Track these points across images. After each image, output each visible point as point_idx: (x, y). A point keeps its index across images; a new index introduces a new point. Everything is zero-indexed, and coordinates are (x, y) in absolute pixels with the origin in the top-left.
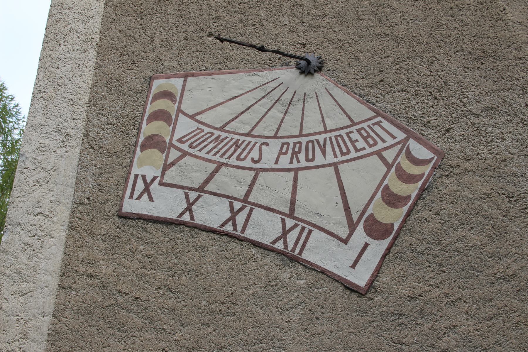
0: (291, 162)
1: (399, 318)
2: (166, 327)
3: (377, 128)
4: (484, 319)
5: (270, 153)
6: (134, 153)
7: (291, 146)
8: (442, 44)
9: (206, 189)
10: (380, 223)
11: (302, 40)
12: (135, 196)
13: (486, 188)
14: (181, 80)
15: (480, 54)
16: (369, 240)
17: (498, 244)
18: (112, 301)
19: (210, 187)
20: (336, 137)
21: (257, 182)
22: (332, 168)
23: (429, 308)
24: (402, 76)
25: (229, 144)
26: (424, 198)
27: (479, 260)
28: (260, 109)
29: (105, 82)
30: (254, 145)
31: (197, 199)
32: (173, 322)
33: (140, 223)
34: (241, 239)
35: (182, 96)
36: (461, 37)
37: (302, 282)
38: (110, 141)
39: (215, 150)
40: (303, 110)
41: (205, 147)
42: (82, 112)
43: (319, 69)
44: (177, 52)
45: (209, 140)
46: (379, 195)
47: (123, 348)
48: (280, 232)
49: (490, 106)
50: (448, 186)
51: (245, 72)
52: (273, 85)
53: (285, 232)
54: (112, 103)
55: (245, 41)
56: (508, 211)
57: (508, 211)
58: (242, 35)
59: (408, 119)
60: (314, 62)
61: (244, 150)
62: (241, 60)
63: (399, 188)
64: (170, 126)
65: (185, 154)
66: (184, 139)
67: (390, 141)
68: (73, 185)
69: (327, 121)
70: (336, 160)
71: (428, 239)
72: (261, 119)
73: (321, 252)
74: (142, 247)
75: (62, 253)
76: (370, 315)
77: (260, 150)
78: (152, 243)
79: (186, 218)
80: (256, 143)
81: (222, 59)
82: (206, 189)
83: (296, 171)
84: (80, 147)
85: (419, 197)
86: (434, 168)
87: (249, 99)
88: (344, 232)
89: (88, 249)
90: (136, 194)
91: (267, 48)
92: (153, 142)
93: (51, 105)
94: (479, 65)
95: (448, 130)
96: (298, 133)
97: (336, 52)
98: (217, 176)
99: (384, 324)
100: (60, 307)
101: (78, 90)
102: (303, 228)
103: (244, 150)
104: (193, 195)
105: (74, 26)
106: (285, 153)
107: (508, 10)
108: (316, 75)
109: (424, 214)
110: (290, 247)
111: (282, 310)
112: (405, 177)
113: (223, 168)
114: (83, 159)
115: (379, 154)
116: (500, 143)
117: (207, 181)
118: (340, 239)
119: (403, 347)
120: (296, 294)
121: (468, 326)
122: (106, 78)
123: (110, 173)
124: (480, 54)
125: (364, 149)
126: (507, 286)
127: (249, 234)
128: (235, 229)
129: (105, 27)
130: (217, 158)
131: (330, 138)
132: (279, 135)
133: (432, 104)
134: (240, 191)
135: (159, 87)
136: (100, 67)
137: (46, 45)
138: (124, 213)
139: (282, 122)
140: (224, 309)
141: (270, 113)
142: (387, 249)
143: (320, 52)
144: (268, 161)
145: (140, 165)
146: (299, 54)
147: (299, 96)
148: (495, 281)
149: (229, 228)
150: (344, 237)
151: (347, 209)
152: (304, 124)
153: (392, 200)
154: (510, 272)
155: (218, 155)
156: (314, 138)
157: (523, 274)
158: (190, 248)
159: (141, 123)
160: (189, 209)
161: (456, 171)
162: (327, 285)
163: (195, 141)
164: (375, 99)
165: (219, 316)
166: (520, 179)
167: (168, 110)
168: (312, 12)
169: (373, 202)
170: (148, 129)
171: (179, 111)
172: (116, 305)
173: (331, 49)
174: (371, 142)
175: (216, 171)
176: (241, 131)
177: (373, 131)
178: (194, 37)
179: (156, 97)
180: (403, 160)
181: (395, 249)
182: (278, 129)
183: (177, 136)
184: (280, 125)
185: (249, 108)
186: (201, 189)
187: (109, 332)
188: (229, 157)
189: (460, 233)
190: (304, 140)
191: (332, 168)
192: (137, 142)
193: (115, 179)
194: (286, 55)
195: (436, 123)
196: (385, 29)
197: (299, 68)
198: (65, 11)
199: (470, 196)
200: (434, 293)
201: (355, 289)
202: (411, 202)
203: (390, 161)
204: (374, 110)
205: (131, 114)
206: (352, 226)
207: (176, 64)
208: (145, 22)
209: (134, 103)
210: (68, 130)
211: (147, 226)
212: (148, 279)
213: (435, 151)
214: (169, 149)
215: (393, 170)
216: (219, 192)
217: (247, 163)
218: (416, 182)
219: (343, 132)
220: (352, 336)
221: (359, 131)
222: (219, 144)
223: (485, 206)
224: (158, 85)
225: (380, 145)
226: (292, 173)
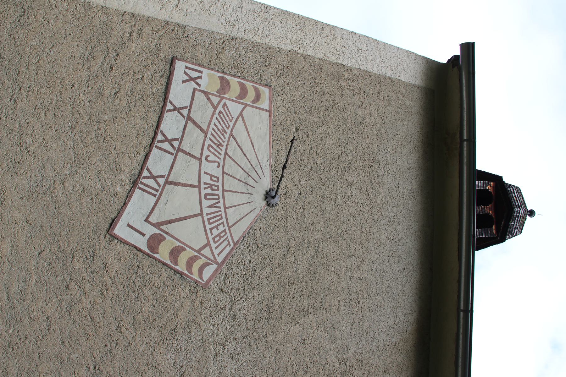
0: (205, 183)
1: (91, 256)
2: (90, 88)
3: (226, 243)
4: (90, 313)
5: (212, 168)
6: (218, 71)
7: (216, 184)
8: (279, 286)
9: (189, 122)
10: (159, 245)
11: (289, 193)
12: (187, 71)
13: (181, 314)
14: (267, 108)
15: (271, 310)
16: (147, 236)
17: (143, 322)
18: (111, 50)
19: (190, 124)
20: (221, 215)
21: (192, 159)
22: (199, 212)
23: (98, 276)
24: (260, 260)
25: (220, 139)
26: (175, 275)
27: (131, 310)
28: (243, 162)
29: (269, 54)
30: (218, 158)
31: (182, 115)
32: (93, 94)
33: (167, 73)
34: (151, 146)
35: (256, 108)
36: (283, 298)
37: (118, 189)
38: (228, 55)
39: (216, 130)
40: (241, 193)
41: (219, 122)
42: (249, 37)
43: (269, 205)
44: (287, 106)
45: (224, 126)
46: (179, 244)
47: (76, 56)
48: (155, 174)
49: (237, 317)
50: (183, 291)
51: (270, 153)
52: (260, 172)
53: (155, 178)
54: (254, 58)
55: (292, 153)
56: (165, 329)
57: (165, 329)
58: (295, 152)
59: (231, 264)
60: (273, 201)
61: (215, 150)
62: (278, 151)
63: (183, 258)
64: (236, 98)
65: (215, 108)
66: (225, 108)
67: (216, 252)
68: (198, 27)
69: (233, 209)
70: (205, 215)
71: (147, 277)
72: (236, 163)
73: (140, 202)
74: (149, 73)
75: (149, 15)
76: (93, 237)
77: (215, 162)
78: (152, 81)
79: (169, 107)
80: (220, 159)
81: (280, 137)
82: (189, 122)
83: (199, 187)
84: (225, 33)
85: (176, 271)
86: (196, 282)
87: (251, 155)
88: (152, 219)
89: (151, 34)
90: (188, 71)
91: (285, 170)
92: (225, 86)
93: (256, 15)
94: (264, 309)
95: (222, 290)
96: (225, 188)
97: (280, 216)
98: (198, 130)
99: (87, 246)
100: (109, 12)
101: (265, 35)
102: (157, 191)
103: (215, 150)
104: (185, 112)
105: (309, 36)
106: (211, 179)
107: (297, 325)
108: (265, 202)
109: (165, 275)
110: (144, 181)
111: (98, 174)
112: (190, 263)
113: (203, 135)
114: (216, 35)
115: (208, 244)
116: (212, 323)
117: (194, 123)
118: (149, 216)
119: (71, 259)
120: (110, 184)
121: (86, 303)
122: (272, 55)
123: (205, 53)
124: (271, 310)
125: (212, 234)
126: (114, 328)
127: (155, 151)
128: (159, 142)
129: (306, 58)
130: (211, 130)
131: (220, 211)
132: (225, 175)
133: (240, 280)
134: (186, 146)
135: (264, 92)
136: (280, 51)
137: (297, 16)
138: (175, 62)
139: (234, 177)
140: (101, 132)
141: (241, 169)
142: (140, 249)
143: (280, 205)
144: (206, 167)
145: (209, 75)
146: (280, 190)
147: (251, 190)
148: (117, 320)
149: (160, 137)
150: (150, 219)
151: (170, 222)
152: (231, 193)
153: (175, 253)
154: (123, 330)
155: (213, 132)
156: (221, 199)
157: (122, 338)
158: (147, 108)
159: (239, 77)
160: (175, 109)
161: (194, 296)
162: (116, 207)
163: (224, 115)
164: (246, 242)
165: (95, 128)
166: (187, 336)
167: (247, 97)
168: (307, 200)
169: (174, 240)
170: (234, 82)
171: (246, 105)
172: (108, 53)
173: (281, 213)
174: (216, 239)
175: (201, 129)
176: (229, 148)
177: (224, 241)
178: (296, 118)
179: (256, 89)
180: (203, 260)
181: (140, 254)
182: (229, 175)
183: (228, 103)
184: (231, 176)
185: (245, 154)
186: (189, 118)
187: (88, 46)
188: (211, 139)
189: (151, 298)
190: (220, 193)
191: (199, 212)
192: (226, 74)
193: (201, 57)
194: (279, 183)
195: (227, 283)
196: (292, 249)
197: (270, 191)
198: (318, 31)
199: (176, 305)
200: (109, 281)
201: (112, 227)
202: (173, 266)
203: (202, 252)
204: (238, 241)
205: (246, 71)
206: (157, 225)
207: (278, 105)
208: (308, 85)
209: (253, 73)
210: (237, 26)
211: (164, 78)
212: (126, 77)
213: (208, 282)
214: (219, 97)
215: (196, 254)
216: (186, 131)
217: (206, 152)
218: (187, 270)
219: (224, 220)
220: (78, 224)
221: (225, 231)
222: (221, 132)
223: (169, 315)
224: (265, 91)
225: (214, 245)
226: (197, 184)
